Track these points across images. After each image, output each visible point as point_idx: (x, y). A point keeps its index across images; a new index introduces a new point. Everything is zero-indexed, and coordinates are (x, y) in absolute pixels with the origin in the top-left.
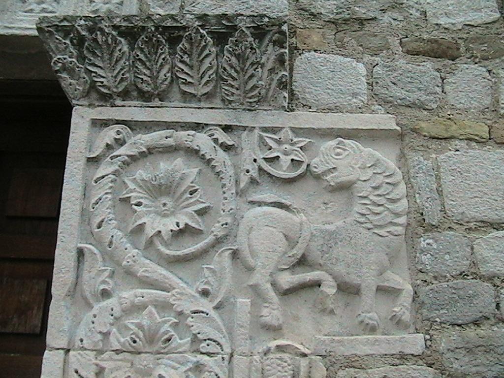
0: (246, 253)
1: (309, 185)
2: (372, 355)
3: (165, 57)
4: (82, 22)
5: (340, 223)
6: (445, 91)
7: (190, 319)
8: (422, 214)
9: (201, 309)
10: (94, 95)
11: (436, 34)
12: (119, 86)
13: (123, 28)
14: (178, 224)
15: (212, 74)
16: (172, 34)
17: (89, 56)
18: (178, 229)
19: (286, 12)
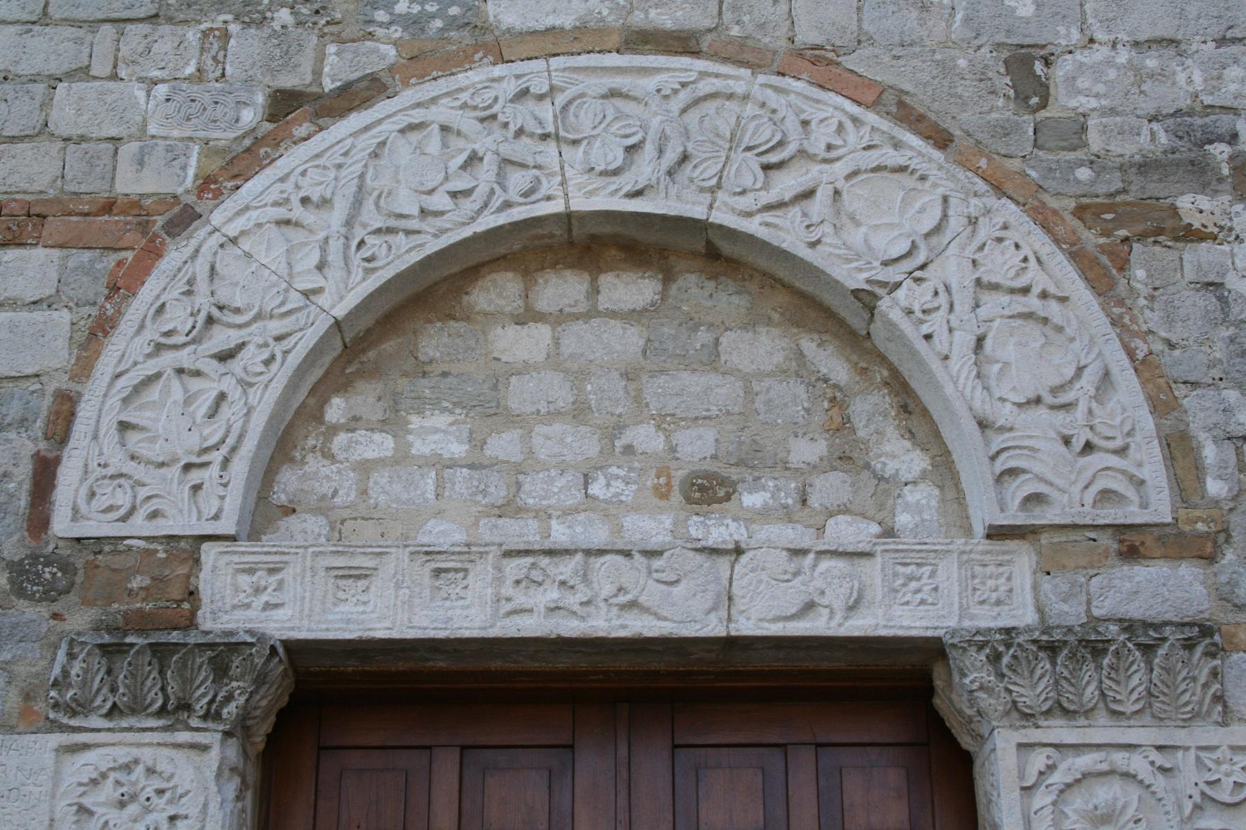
4: (998, 636)
10: (1015, 715)
17: (1009, 673)
19: (1206, 605)
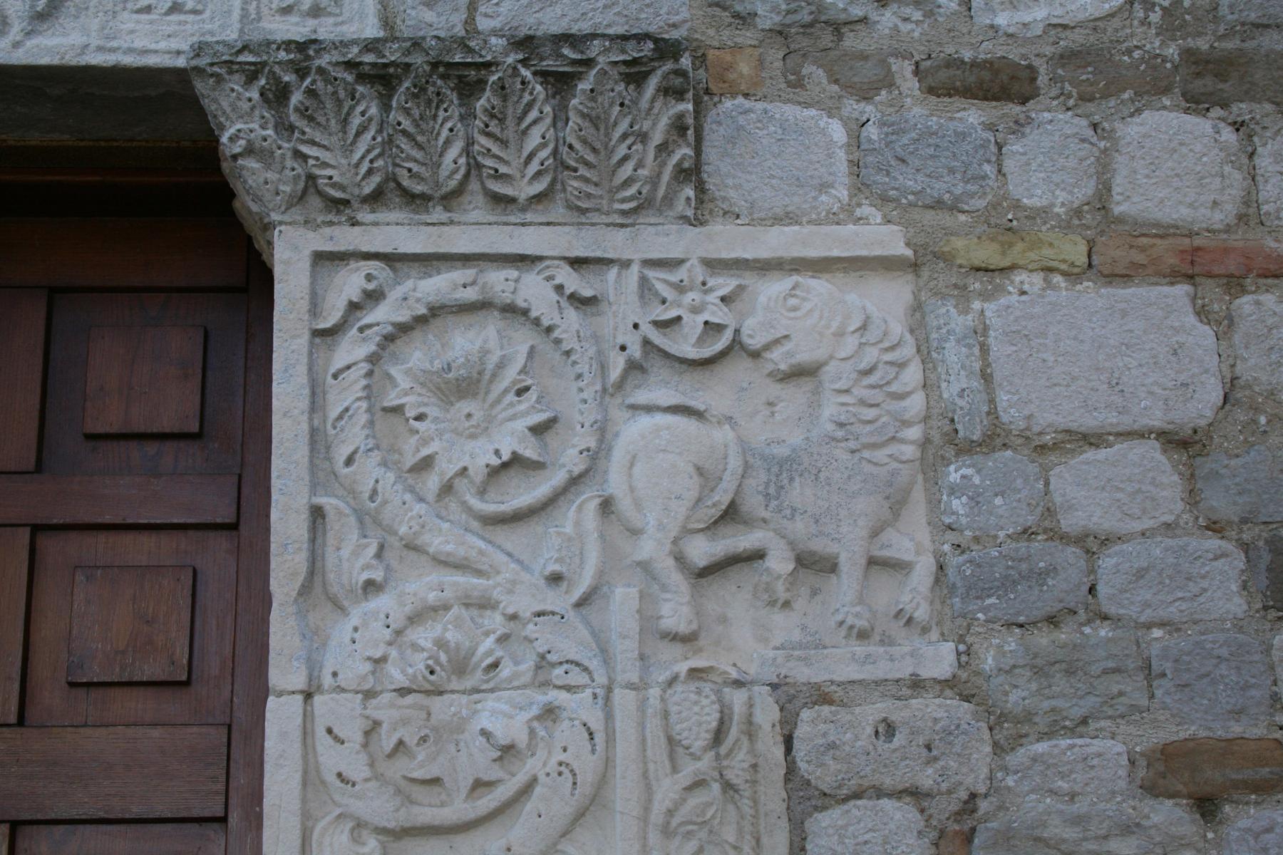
0: (624, 504)
1: (738, 369)
2: (860, 681)
3: (455, 126)
4: (282, 55)
5: (1193, 728)
6: (1005, 170)
7: (531, 626)
8: (952, 420)
9: (549, 608)
10: (315, 202)
11: (989, 49)
12: (364, 183)
13: (367, 68)
14: (497, 452)
15: (547, 158)
16: (458, 75)
18: (499, 462)
